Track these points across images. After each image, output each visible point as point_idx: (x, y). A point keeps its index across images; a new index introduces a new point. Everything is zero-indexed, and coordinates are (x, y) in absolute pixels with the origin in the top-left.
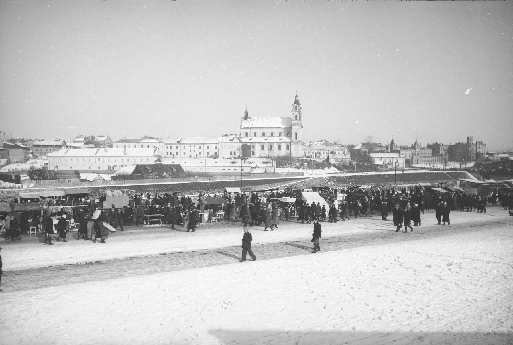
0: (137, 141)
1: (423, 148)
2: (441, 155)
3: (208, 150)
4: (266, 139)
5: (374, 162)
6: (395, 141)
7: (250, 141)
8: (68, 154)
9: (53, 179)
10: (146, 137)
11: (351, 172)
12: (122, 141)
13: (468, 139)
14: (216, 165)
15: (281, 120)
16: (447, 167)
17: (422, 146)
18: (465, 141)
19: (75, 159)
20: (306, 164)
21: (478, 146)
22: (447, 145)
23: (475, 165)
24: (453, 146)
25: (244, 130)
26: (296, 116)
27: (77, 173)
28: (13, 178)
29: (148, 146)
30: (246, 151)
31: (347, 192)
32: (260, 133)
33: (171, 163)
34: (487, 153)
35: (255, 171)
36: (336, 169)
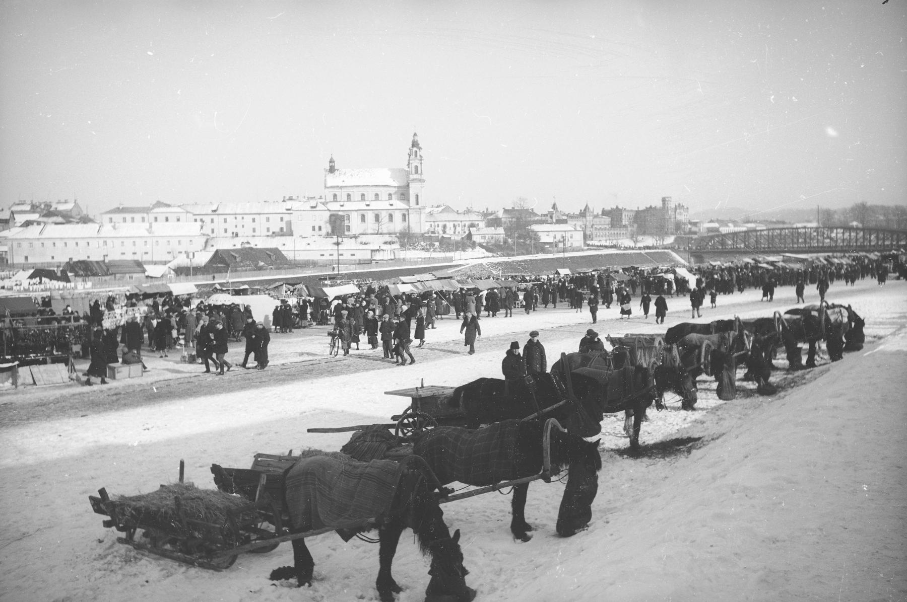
0: (146, 210)
1: (596, 216)
2: (625, 226)
3: (268, 225)
4: (368, 205)
5: (540, 239)
6: (589, 206)
7: (342, 208)
8: (46, 234)
9: (107, 275)
10: (159, 204)
11: (508, 255)
12: (118, 210)
13: (664, 200)
14: (308, 247)
15: (390, 173)
16: (639, 245)
17: (595, 213)
18: (659, 204)
19: (59, 244)
20: (437, 244)
21: (678, 211)
22: (632, 211)
23: (676, 240)
24: (643, 211)
25: (331, 190)
26: (416, 167)
27: (139, 265)
28: (59, 274)
29: (167, 220)
30: (337, 226)
31: (198, 355)
32: (356, 195)
33: (231, 247)
34: (690, 223)
35: (378, 256)
36: (484, 250)
